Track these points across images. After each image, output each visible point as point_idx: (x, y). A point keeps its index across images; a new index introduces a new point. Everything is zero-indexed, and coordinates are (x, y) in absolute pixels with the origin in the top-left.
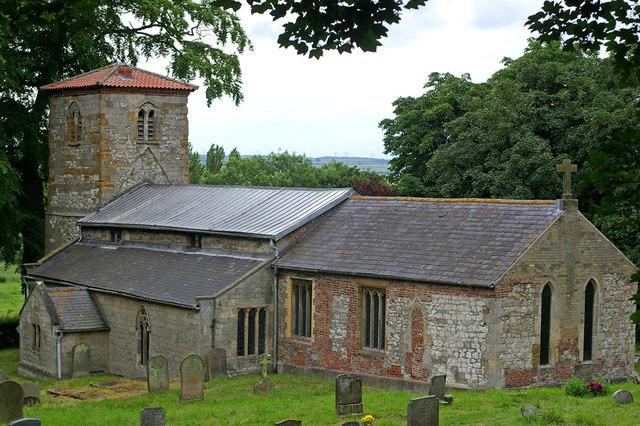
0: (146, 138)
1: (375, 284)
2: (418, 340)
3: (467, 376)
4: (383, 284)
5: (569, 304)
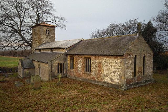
2: (100, 70)
3: (115, 81)
4: (90, 56)
5: (140, 61)
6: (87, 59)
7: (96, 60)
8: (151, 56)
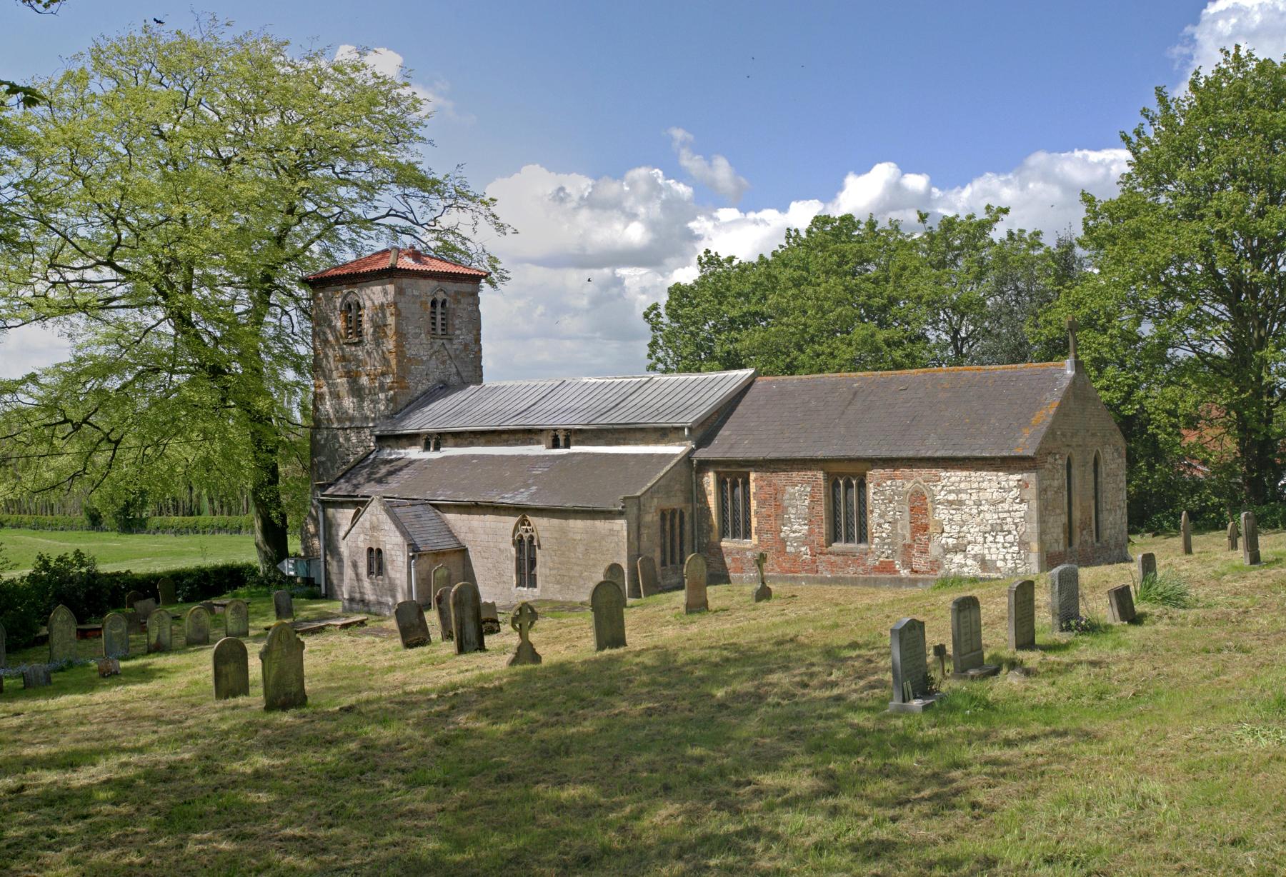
0: (440, 332)
1: (850, 469)
2: (920, 528)
3: (1000, 564)
4: (858, 468)
7: (899, 482)
8: (1120, 456)
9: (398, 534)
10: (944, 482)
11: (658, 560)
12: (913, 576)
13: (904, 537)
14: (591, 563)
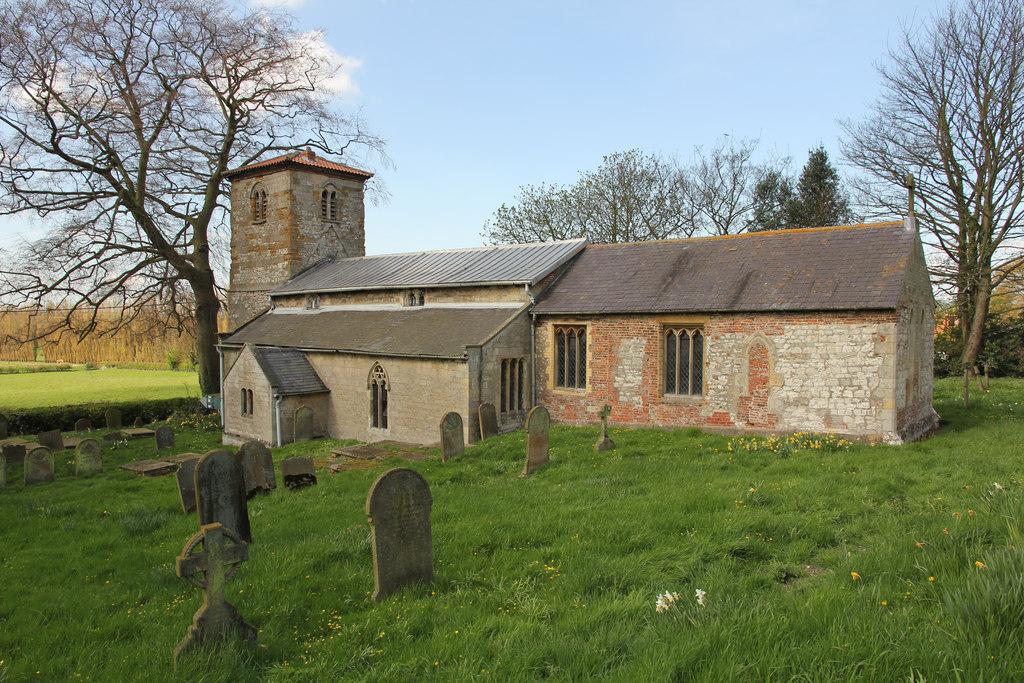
6: (677, 333)
7: (739, 335)
9: (264, 377)
10: (789, 335)
11: (498, 407)
12: (749, 428)
13: (741, 390)
14: (435, 408)
